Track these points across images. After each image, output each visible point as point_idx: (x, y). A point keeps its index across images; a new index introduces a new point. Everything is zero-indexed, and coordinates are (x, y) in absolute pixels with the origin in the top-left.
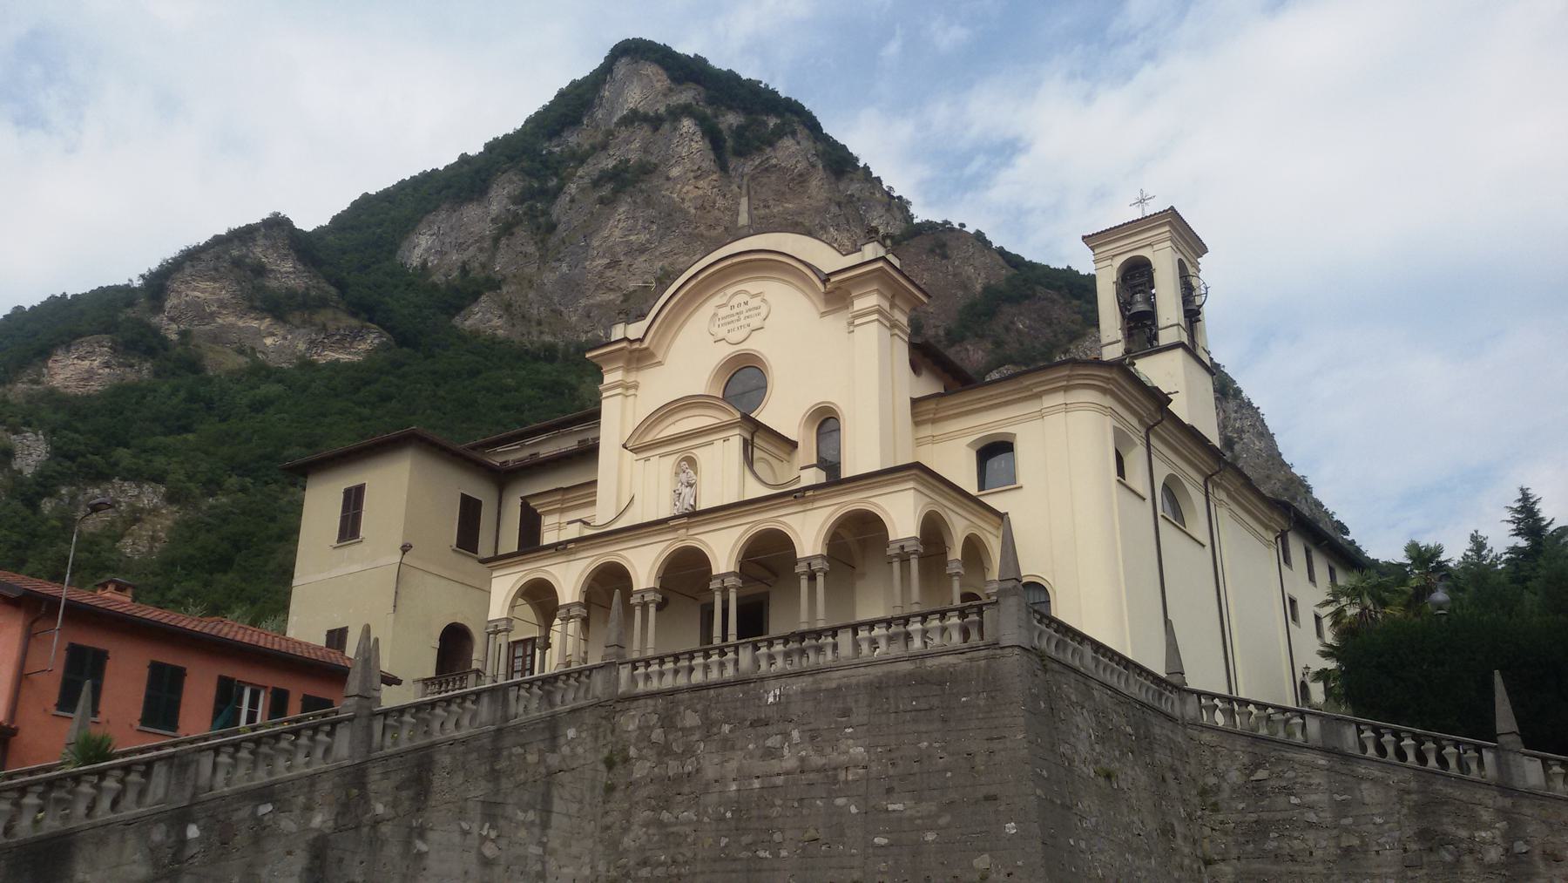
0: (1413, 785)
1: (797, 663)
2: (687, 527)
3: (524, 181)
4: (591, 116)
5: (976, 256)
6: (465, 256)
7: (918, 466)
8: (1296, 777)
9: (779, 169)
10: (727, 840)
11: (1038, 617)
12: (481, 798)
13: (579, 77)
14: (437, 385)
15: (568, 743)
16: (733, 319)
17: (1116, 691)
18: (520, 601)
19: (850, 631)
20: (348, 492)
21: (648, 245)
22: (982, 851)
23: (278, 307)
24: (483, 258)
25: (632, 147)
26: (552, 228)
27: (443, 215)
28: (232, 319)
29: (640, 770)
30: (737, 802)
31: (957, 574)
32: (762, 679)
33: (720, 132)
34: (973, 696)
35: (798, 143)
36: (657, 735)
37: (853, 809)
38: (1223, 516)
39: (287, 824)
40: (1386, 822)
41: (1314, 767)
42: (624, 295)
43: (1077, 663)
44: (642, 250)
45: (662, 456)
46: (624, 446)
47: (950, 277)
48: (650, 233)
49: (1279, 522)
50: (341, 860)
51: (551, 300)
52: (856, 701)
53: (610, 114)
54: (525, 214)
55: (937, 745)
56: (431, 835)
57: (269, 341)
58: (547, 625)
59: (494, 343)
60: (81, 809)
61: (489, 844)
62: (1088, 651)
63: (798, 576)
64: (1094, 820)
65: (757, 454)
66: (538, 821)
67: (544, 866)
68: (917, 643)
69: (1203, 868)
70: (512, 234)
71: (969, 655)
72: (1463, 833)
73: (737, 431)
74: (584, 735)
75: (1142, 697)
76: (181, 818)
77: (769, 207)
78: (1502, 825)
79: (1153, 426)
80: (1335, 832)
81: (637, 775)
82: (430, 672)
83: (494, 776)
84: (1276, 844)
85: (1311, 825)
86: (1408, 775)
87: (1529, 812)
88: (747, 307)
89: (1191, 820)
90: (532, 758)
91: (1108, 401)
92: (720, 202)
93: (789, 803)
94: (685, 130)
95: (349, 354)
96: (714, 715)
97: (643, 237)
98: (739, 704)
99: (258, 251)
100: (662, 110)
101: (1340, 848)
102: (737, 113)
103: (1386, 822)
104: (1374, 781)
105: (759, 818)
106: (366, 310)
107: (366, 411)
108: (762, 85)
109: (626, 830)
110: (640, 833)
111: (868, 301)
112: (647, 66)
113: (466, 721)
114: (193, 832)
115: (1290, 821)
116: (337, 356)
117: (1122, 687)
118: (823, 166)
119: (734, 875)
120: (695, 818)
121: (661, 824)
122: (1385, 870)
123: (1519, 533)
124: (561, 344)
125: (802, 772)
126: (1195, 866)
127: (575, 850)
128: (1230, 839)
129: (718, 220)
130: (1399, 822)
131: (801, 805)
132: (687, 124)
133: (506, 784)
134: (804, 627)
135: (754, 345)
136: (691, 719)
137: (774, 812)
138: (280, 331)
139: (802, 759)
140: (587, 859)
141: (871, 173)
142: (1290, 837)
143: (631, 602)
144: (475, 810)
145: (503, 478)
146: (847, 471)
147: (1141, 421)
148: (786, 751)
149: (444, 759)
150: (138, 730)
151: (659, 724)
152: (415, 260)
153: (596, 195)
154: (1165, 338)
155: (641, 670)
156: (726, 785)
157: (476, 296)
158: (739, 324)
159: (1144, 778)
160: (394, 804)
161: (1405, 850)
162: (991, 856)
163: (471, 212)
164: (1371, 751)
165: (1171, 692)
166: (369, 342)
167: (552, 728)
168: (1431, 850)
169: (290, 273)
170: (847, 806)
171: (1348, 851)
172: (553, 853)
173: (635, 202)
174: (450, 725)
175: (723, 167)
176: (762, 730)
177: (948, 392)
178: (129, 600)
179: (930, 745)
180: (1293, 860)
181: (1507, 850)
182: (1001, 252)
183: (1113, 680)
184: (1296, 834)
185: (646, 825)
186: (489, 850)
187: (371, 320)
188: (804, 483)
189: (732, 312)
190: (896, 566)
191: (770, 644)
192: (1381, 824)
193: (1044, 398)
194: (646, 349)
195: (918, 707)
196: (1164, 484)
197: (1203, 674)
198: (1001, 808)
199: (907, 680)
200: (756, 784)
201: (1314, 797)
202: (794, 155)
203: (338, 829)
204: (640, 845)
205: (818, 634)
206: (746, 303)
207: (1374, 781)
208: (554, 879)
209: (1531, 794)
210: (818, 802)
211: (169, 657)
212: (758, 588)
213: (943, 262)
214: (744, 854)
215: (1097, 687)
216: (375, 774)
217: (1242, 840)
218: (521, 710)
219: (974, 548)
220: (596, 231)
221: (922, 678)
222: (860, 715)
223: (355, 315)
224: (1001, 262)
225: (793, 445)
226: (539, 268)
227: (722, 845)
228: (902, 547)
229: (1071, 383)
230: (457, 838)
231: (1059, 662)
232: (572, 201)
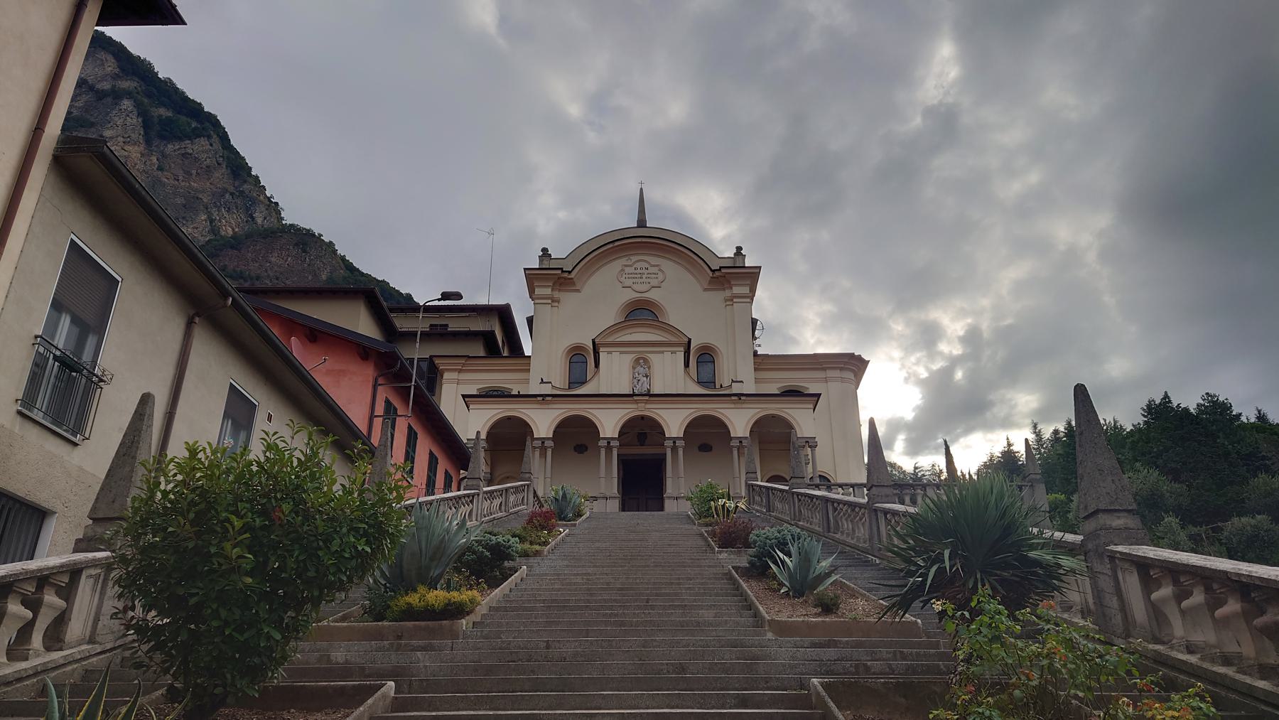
2: (647, 402)
16: (636, 276)
35: (211, 145)
45: (621, 353)
102: (168, 109)
112: (102, 53)
118: (226, 166)
132: (127, 104)
143: (599, 445)
158: (642, 280)
175: (148, 142)
182: (343, 258)
189: (636, 271)
193: (827, 371)
194: (572, 279)
202: (206, 152)
213: (304, 254)
229: (846, 366)
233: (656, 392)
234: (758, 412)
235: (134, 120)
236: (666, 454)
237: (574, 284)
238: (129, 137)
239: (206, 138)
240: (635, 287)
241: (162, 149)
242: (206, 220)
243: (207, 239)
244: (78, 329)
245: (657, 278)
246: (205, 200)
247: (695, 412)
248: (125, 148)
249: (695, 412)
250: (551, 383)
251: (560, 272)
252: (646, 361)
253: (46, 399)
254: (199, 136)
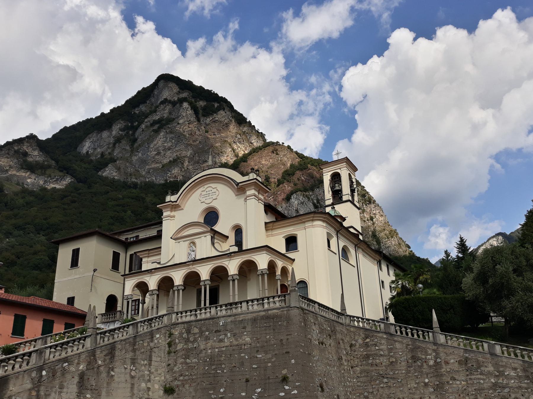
0: (410, 343)
1: (229, 312)
2: (193, 265)
3: (125, 123)
4: (150, 101)
5: (288, 154)
6: (102, 150)
7: (267, 246)
8: (377, 341)
9: (219, 122)
10: (207, 367)
11: (302, 297)
12: (130, 358)
13: (145, 86)
14: (92, 197)
15: (157, 339)
17: (325, 317)
18: (136, 289)
19: (246, 302)
20: (74, 251)
21: (171, 147)
22: (284, 369)
23: (32, 168)
24: (109, 151)
25: (166, 112)
26: (135, 140)
27: (95, 135)
28: (14, 172)
29: (180, 347)
30: (211, 356)
31: (279, 279)
32: (218, 318)
33: (198, 108)
34: (282, 322)
35: (226, 113)
36: (185, 335)
37: (247, 357)
38: (361, 256)
39: (73, 369)
40: (402, 354)
41: (382, 338)
42: (162, 165)
43: (313, 310)
44: (169, 149)
45: (184, 241)
46: (171, 238)
47: (279, 161)
48: (172, 143)
49: (378, 257)
50: (89, 379)
51: (135, 166)
52: (248, 324)
53: (158, 99)
54: (125, 135)
55: (272, 337)
56: (115, 370)
57: (29, 181)
58: (144, 296)
59: (114, 181)
60: (10, 368)
61: (133, 371)
62: (316, 305)
63: (229, 280)
64: (317, 357)
65: (216, 241)
66: (148, 364)
67: (150, 377)
68: (266, 306)
69: (351, 369)
70: (121, 142)
71: (281, 310)
72: (424, 357)
73: (209, 234)
74: (161, 336)
75: (333, 318)
76: (40, 369)
78: (434, 354)
79: (339, 231)
80: (388, 357)
81: (178, 348)
82: (104, 312)
83: (134, 350)
84: (372, 361)
85: (381, 355)
86: (409, 340)
87: (441, 350)
88: (212, 192)
89: (347, 354)
90: (145, 344)
91: (324, 225)
92: (198, 133)
93: (227, 356)
94: (185, 106)
95: (59, 185)
96: (204, 329)
97: (170, 144)
98: (211, 325)
99: (25, 148)
100: (176, 99)
101: (390, 362)
103: (402, 354)
104: (399, 342)
105: (217, 361)
106: (66, 170)
107: (66, 207)
108: (212, 92)
109: (175, 365)
110: (180, 366)
111: (251, 192)
113: (125, 334)
114: (44, 373)
115: (376, 354)
116: (55, 186)
117: (327, 316)
118: (235, 121)
119: (210, 378)
120: (197, 361)
121: (187, 363)
122: (402, 368)
123: (460, 252)
124: (139, 182)
125: (231, 346)
126: (348, 368)
127: (159, 372)
128: (359, 360)
129: (197, 139)
130: (406, 354)
131: (230, 356)
132: (185, 105)
133: (138, 353)
134: (231, 301)
135: (214, 204)
136: (196, 330)
137: (222, 359)
138: (33, 177)
139: (231, 342)
140: (163, 374)
141: (251, 124)
142: (376, 359)
144: (129, 362)
145: (126, 245)
146: (244, 248)
147: (335, 229)
148: (226, 340)
149: (119, 346)
150: (11, 337)
151: (185, 332)
152: (84, 151)
153: (152, 129)
154: (345, 198)
155: (180, 315)
156: (207, 351)
157: (106, 165)
158: (209, 197)
159: (333, 343)
160: (104, 361)
161: (408, 362)
162: (287, 370)
163: (105, 134)
164: (399, 333)
165: (342, 316)
166: (67, 181)
167: (151, 335)
168: (415, 362)
169: (37, 155)
170: (245, 356)
171: (392, 362)
172: (152, 373)
173: (166, 132)
174: (120, 335)
175: (199, 120)
176: (218, 334)
177: (277, 220)
178: (3, 292)
179: (270, 337)
180: (377, 365)
181: (435, 361)
183: (324, 314)
184: (377, 358)
185: (182, 363)
186: (133, 373)
187: (67, 173)
188: (231, 251)
190: (260, 277)
191: (221, 306)
192: (401, 355)
193: (306, 223)
195: (266, 326)
196: (342, 248)
197: (353, 310)
198: (290, 355)
199: (263, 317)
200: (217, 350)
201: (382, 347)
202: (224, 117)
203: (87, 369)
204: (180, 370)
205: (236, 303)
206: (211, 191)
207: (399, 342)
208: (153, 381)
209: (442, 345)
210: (236, 355)
211: (21, 312)
212: (215, 284)
213: (277, 156)
214: (213, 372)
215: (319, 317)
216: (98, 352)
217: (362, 360)
218: (142, 330)
219: (284, 270)
220: (152, 142)
221: (267, 317)
222: (249, 328)
223: (61, 171)
224: (297, 156)
225: (227, 237)
226: (130, 155)
227: (206, 369)
228: (262, 272)
230: (123, 370)
231: (308, 311)
232: (143, 131)
234: (241, 260)
235: (190, 112)
236: (201, 288)
237: (180, 206)
238: (190, 121)
241: (205, 121)
242: (231, 151)
243: (234, 160)
245: (216, 194)
246: (229, 141)
248: (189, 126)
249: (214, 265)
253: (276, 227)
254: (219, 110)
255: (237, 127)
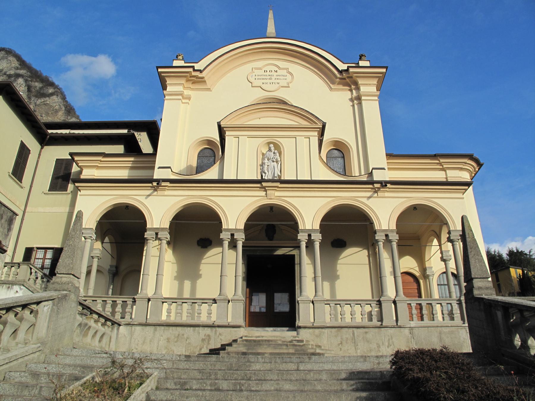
16: (259, 77)
77: (42, 116)
94: (19, 82)
158: (271, 81)
194: (203, 78)
202: (55, 103)
233: (287, 178)
239: (56, 96)
240: (264, 86)
241: (36, 101)
244: (288, 294)
247: (333, 201)
250: (169, 168)
251: (191, 70)
252: (277, 147)
255: (65, 116)
